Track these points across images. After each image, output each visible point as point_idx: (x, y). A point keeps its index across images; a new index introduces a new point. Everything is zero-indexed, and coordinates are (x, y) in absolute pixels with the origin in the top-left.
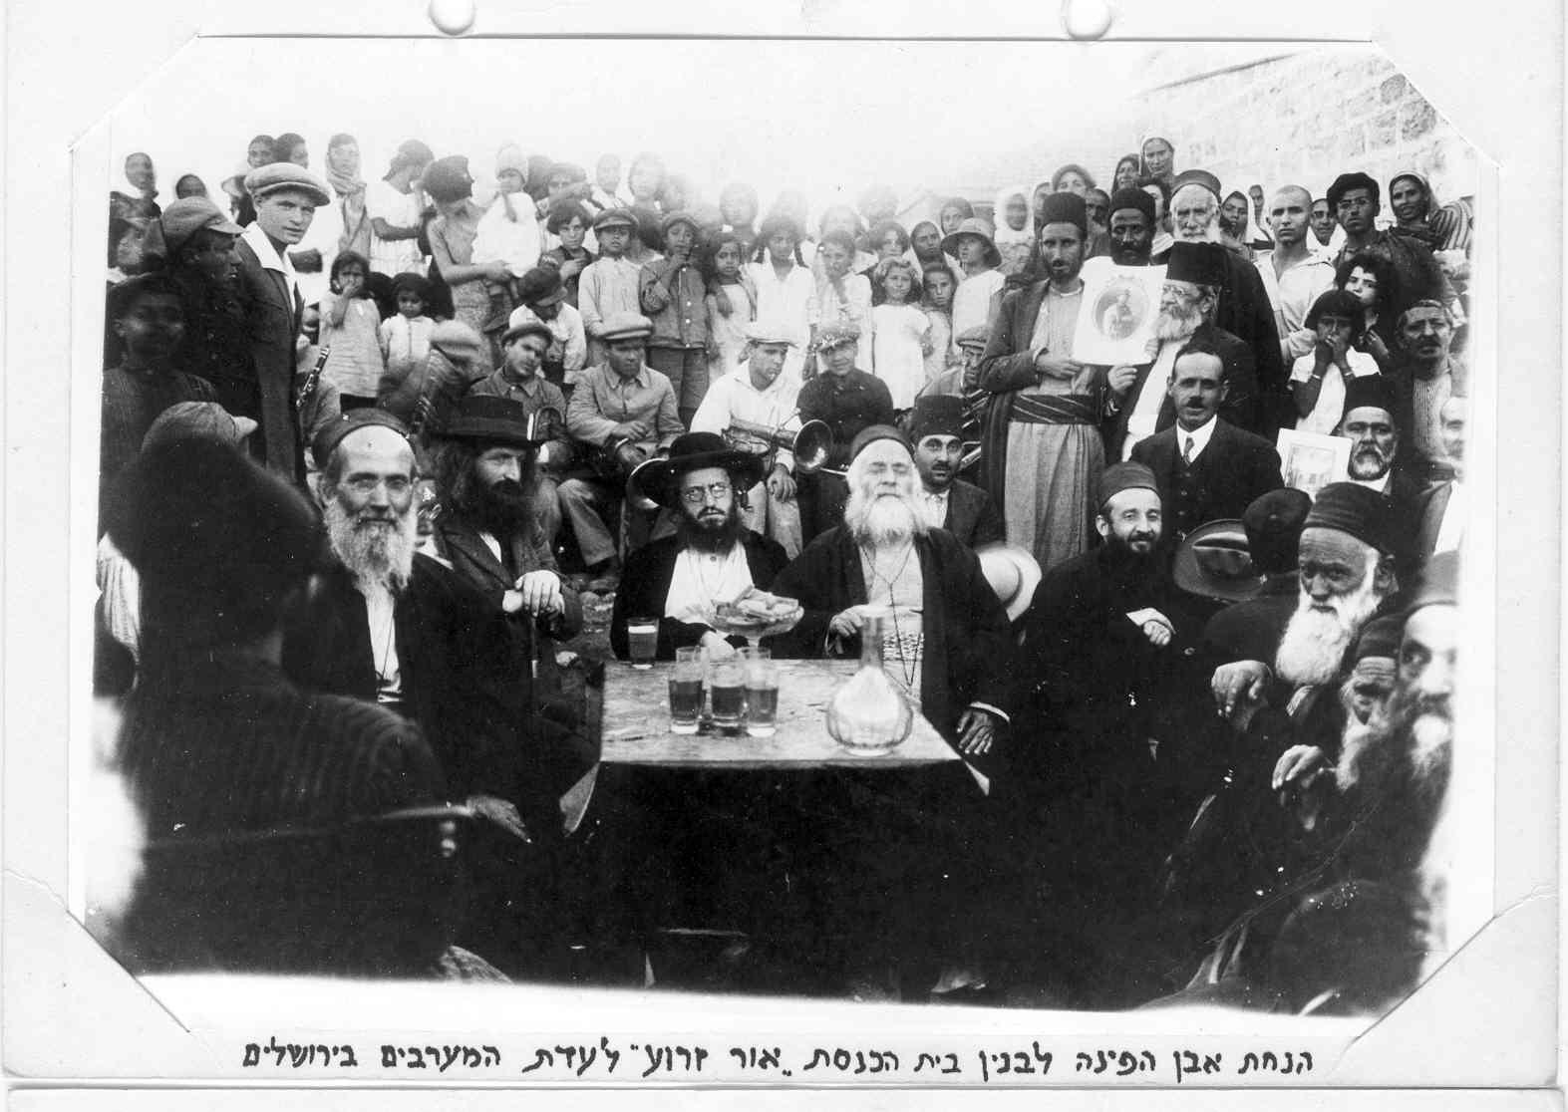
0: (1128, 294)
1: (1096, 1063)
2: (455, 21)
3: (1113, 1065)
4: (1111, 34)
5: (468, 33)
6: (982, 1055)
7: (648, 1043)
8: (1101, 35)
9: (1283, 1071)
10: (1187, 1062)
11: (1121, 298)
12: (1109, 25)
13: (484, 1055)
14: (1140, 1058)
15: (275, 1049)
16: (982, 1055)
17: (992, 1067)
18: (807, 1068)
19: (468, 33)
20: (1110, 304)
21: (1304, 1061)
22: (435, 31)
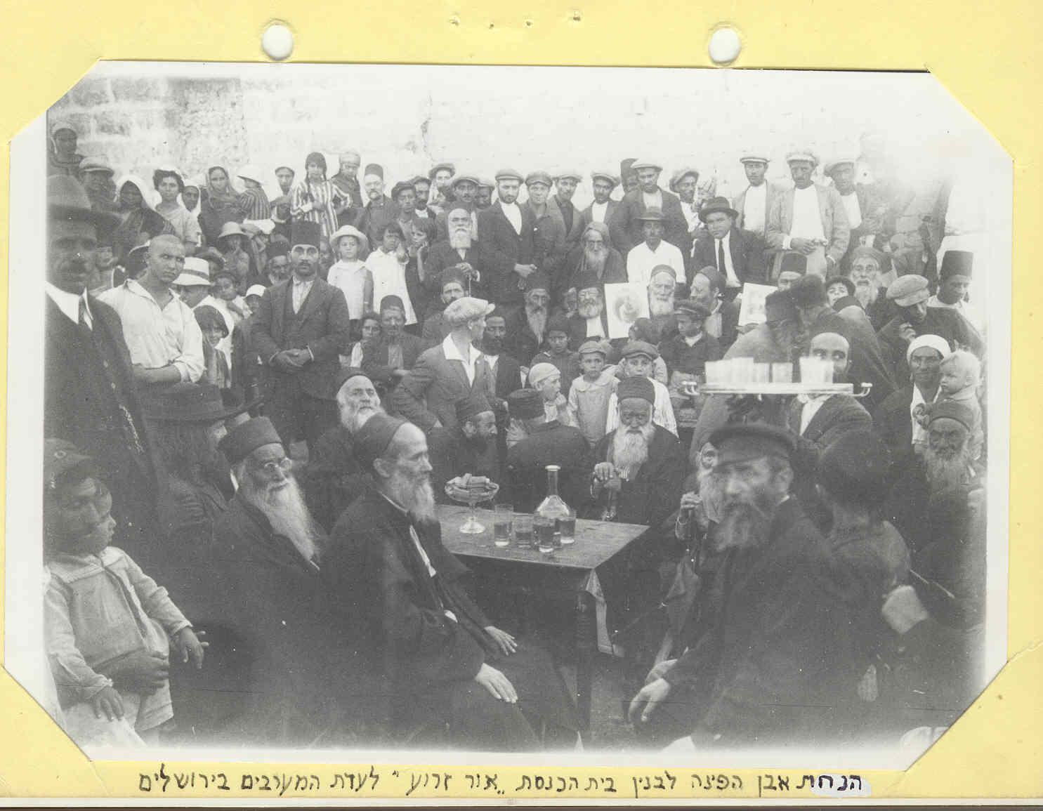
0: (628, 299)
1: (705, 783)
2: (278, 52)
3: (715, 783)
4: (294, 57)
5: (290, 59)
6: (634, 779)
7: (274, 773)
8: (731, 61)
9: (839, 789)
10: (766, 782)
11: (626, 301)
12: (739, 51)
13: (310, 780)
14: (732, 780)
15: (163, 776)
16: (634, 779)
17: (640, 786)
18: (798, 787)
19: (737, 64)
20: (621, 305)
21: (574, 783)
22: (263, 58)
